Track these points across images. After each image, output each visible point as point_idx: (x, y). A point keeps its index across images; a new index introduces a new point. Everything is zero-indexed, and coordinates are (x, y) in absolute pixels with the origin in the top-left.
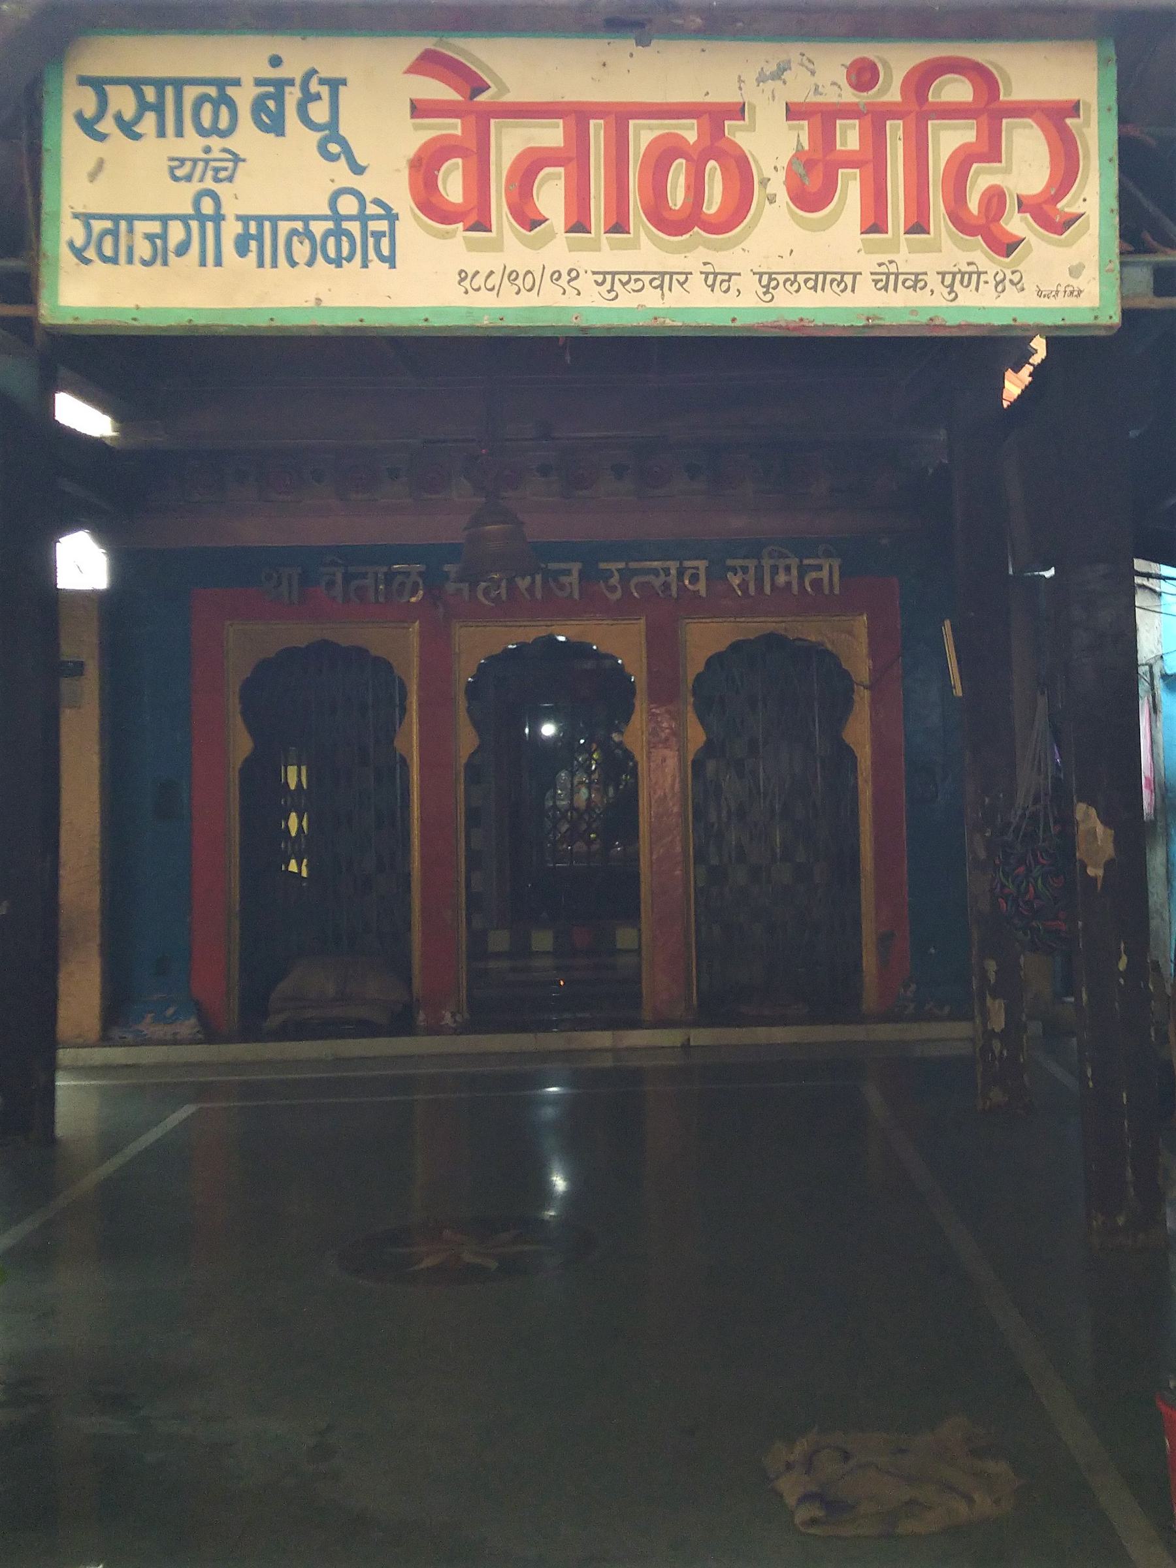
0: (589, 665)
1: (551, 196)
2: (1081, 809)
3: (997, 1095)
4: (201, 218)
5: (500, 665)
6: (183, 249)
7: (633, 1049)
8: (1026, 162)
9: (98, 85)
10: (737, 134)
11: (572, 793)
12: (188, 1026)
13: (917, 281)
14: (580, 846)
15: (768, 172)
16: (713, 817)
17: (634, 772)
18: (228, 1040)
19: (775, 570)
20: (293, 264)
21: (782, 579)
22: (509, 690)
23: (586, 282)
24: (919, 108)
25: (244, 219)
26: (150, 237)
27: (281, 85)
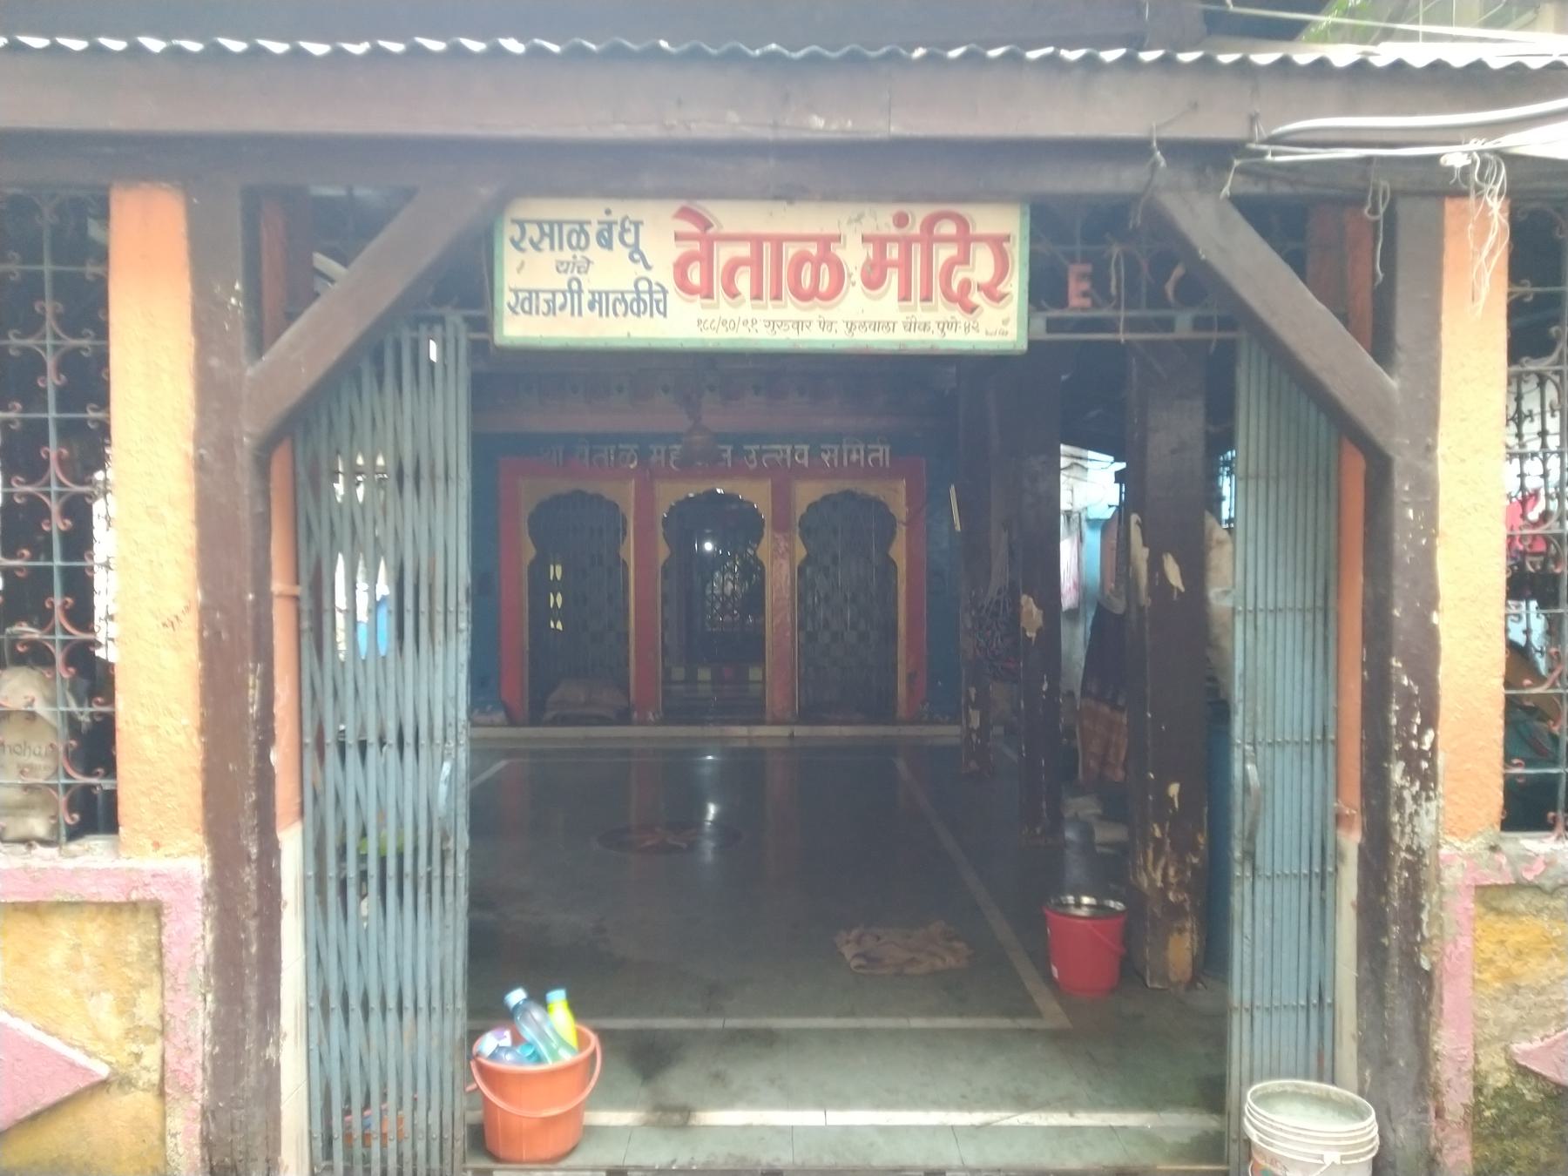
0: (734, 507)
1: (743, 282)
2: (1024, 598)
3: (973, 765)
4: (572, 292)
5: (682, 509)
6: (563, 307)
7: (759, 737)
8: (982, 266)
9: (521, 224)
10: (838, 251)
11: (723, 586)
12: (500, 716)
13: (926, 327)
14: (728, 618)
15: (852, 270)
16: (809, 601)
17: (762, 574)
18: (523, 725)
19: (850, 452)
20: (616, 314)
21: (854, 457)
22: (690, 519)
23: (760, 326)
24: (929, 237)
25: (593, 293)
26: (547, 302)
27: (610, 225)
